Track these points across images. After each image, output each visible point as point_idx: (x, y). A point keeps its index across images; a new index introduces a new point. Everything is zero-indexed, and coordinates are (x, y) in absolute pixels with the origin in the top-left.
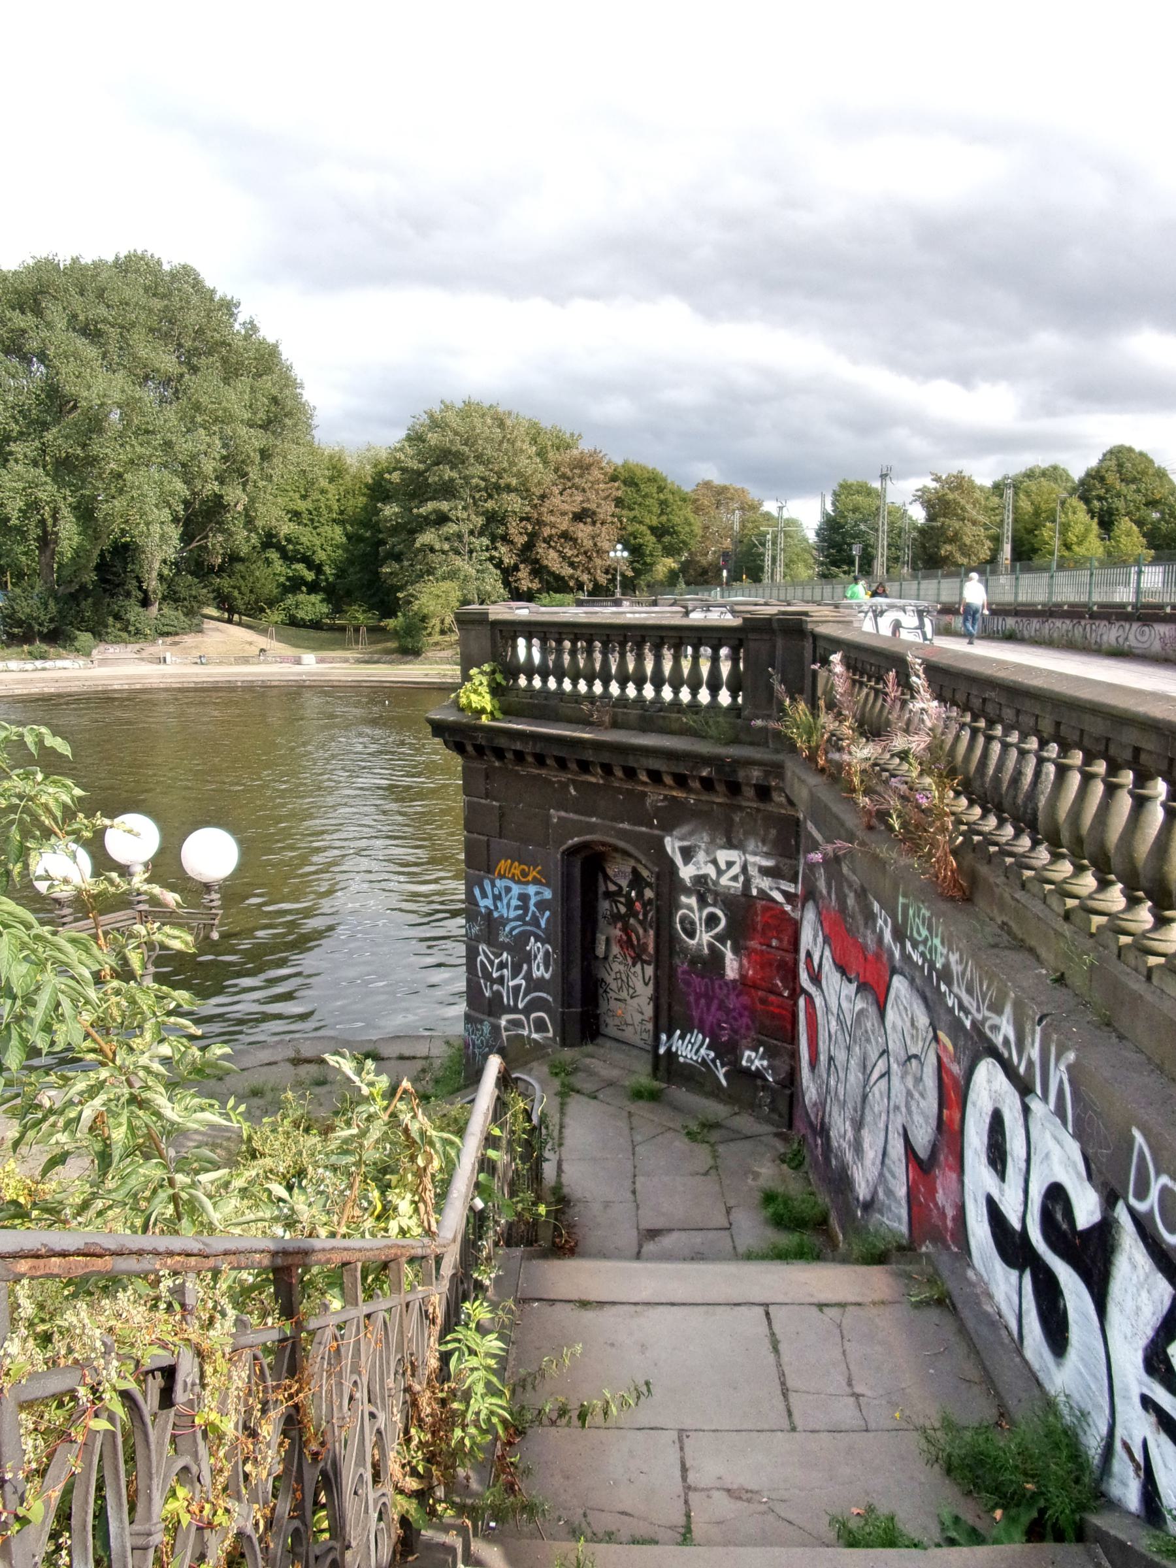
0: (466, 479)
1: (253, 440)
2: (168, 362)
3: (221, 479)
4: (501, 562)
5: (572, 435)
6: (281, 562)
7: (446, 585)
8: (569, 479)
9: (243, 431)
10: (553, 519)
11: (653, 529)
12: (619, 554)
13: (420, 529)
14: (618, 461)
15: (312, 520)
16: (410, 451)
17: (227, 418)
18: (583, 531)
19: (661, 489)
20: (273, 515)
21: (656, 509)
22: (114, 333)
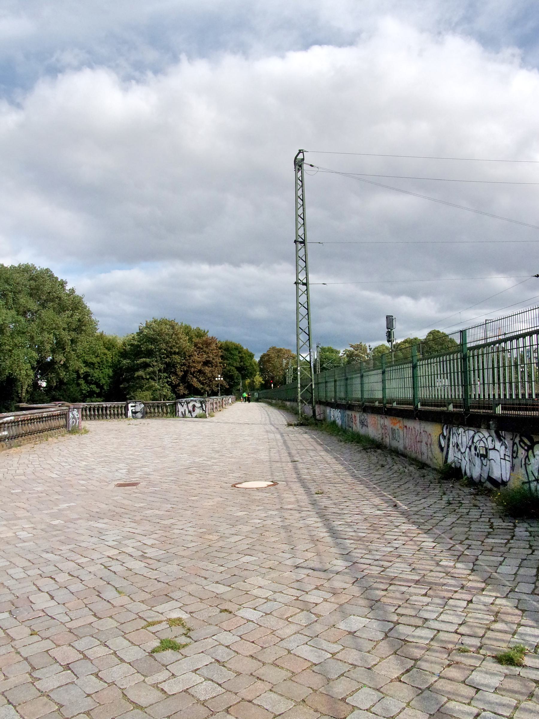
0: (160, 350)
1: (66, 337)
2: (33, 305)
3: (53, 351)
5: (204, 331)
7: (146, 393)
8: (202, 349)
10: (194, 365)
11: (237, 368)
12: (219, 378)
13: (137, 370)
14: (223, 340)
15: (99, 366)
18: (207, 370)
20: (77, 364)
21: (239, 360)
22: (11, 295)
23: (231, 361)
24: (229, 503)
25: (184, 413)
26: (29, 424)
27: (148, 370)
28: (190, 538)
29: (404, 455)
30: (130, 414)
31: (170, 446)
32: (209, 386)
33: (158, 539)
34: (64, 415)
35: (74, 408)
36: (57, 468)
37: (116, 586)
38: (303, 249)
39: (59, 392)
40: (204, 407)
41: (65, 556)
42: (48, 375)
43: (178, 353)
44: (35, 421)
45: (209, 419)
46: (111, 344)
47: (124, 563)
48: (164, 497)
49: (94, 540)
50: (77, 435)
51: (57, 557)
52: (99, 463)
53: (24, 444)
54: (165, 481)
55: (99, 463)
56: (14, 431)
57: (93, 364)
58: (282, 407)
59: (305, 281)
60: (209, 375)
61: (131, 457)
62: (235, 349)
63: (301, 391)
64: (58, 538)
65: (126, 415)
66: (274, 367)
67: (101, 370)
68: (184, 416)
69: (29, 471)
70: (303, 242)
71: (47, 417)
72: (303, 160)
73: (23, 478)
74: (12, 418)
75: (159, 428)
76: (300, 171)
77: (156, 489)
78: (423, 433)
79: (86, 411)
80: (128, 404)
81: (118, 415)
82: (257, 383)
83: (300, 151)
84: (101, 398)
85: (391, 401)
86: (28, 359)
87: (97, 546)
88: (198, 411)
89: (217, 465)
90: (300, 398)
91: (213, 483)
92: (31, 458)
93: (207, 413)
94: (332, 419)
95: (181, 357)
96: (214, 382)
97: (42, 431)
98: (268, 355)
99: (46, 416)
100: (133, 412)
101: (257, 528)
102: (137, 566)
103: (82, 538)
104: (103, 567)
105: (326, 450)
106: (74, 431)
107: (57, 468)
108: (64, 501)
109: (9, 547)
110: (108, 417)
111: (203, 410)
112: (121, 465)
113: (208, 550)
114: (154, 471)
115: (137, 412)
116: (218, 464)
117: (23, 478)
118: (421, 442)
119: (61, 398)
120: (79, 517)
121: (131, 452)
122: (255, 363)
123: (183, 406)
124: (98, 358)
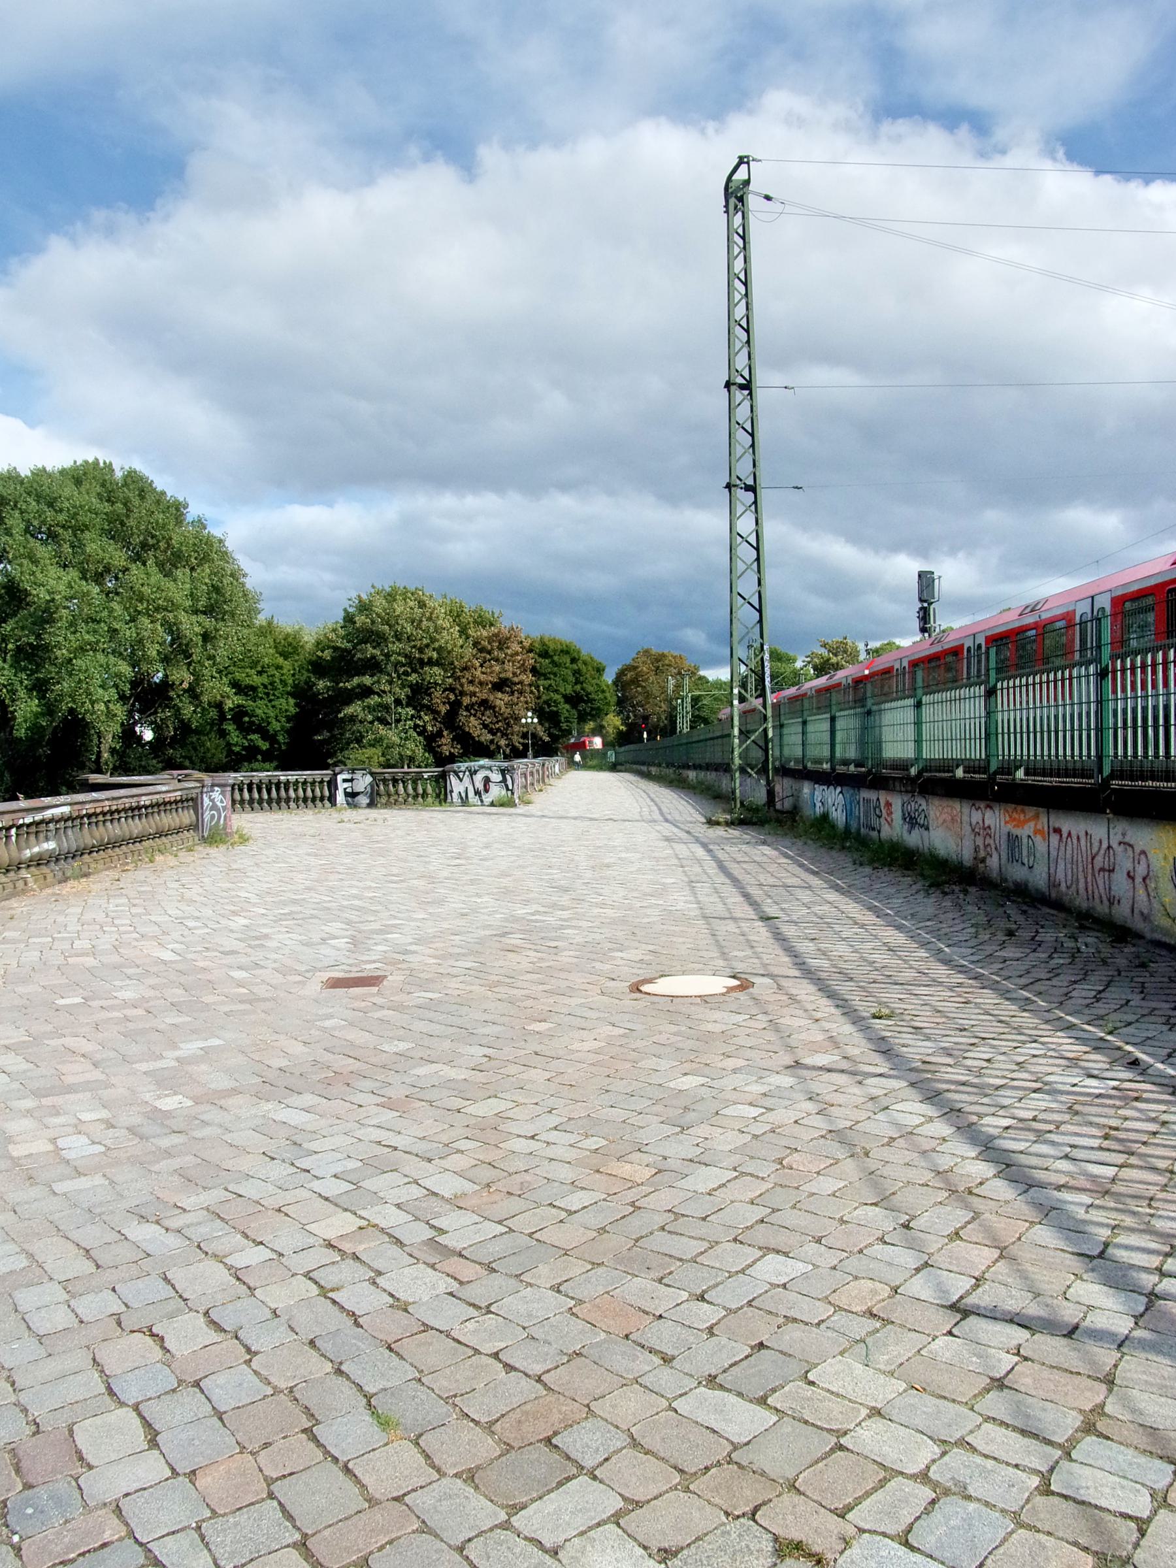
1: (191, 626)
3: (166, 660)
4: (425, 730)
6: (237, 733)
7: (370, 752)
8: (489, 653)
9: (183, 617)
10: (472, 688)
12: (530, 719)
13: (348, 702)
14: (536, 634)
15: (267, 694)
16: (342, 632)
17: (173, 606)
18: (500, 700)
19: (574, 660)
20: (216, 688)
21: (572, 679)
23: (552, 682)
24: (639, 1044)
25: (463, 795)
26: (108, 824)
27: (369, 700)
28: (565, 1173)
29: (1058, 905)
30: (340, 797)
31: (445, 874)
32: (504, 735)
33: (470, 1174)
34: (192, 802)
35: (213, 785)
36: (176, 935)
37: (370, 1389)
38: (747, 404)
39: (179, 750)
40: (509, 782)
41: (196, 1234)
42: (156, 713)
43: (437, 663)
44: (123, 814)
45: (521, 809)
46: (290, 644)
47: (380, 1273)
48: (459, 1022)
49: (278, 1171)
50: (223, 848)
51: (173, 1241)
52: (278, 920)
53: (97, 872)
54: (450, 970)
55: (278, 920)
56: (73, 839)
57: (254, 689)
58: (678, 783)
59: (750, 482)
60: (506, 711)
61: (356, 902)
62: (562, 651)
63: (740, 746)
64: (176, 1163)
65: (332, 799)
66: (648, 695)
67: (270, 701)
68: (465, 801)
69: (105, 942)
70: (747, 386)
71: (152, 806)
72: (747, 182)
73: (89, 961)
74: (66, 810)
75: (406, 828)
76: (740, 213)
77: (430, 995)
78: (1119, 849)
79: (241, 790)
80: (335, 775)
81: (314, 799)
82: (610, 730)
83: (741, 158)
84: (271, 762)
85: (1008, 768)
86: (111, 677)
87: (289, 1197)
88: (496, 792)
89: (575, 927)
90: (737, 761)
91: (578, 979)
92: (111, 907)
93: (516, 796)
94: (819, 810)
95: (446, 671)
96: (516, 728)
97: (140, 839)
98: (635, 668)
99: (148, 803)
100: (347, 794)
101: (755, 1137)
102: (421, 1285)
103: (244, 1164)
104: (315, 1290)
105: (837, 888)
106: (216, 837)
107: (176, 935)
108: (193, 1032)
109: (35, 1192)
110: (292, 804)
111: (508, 789)
112: (335, 927)
113: (636, 1225)
114: (418, 941)
115: (358, 794)
116: (574, 923)
117: (89, 961)
118: (1111, 871)
119: (187, 763)
120: (233, 1084)
121: (354, 891)
122: (608, 686)
123: (461, 780)
124: (265, 675)
